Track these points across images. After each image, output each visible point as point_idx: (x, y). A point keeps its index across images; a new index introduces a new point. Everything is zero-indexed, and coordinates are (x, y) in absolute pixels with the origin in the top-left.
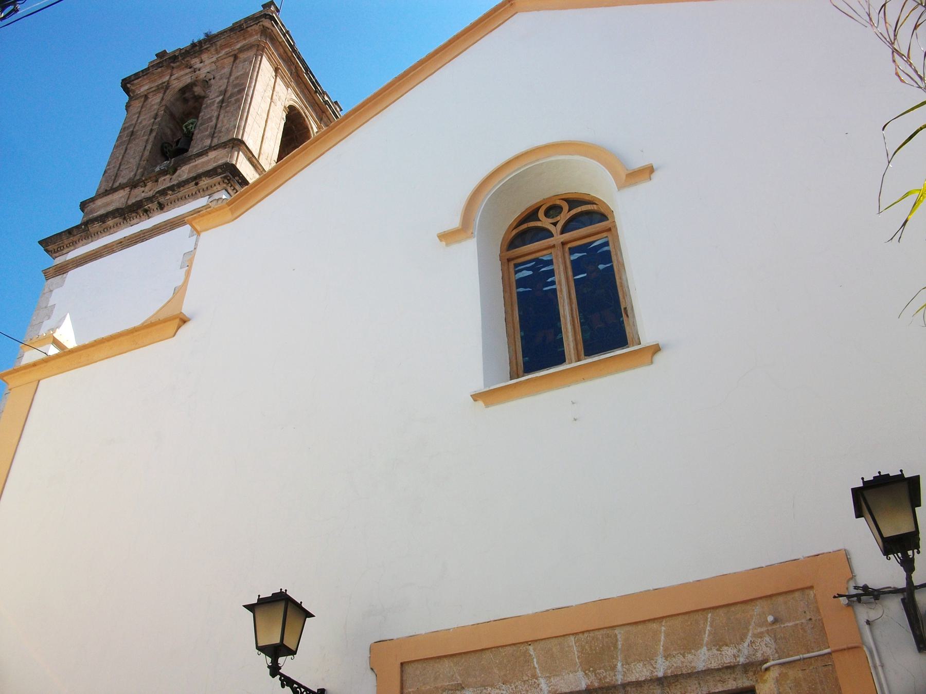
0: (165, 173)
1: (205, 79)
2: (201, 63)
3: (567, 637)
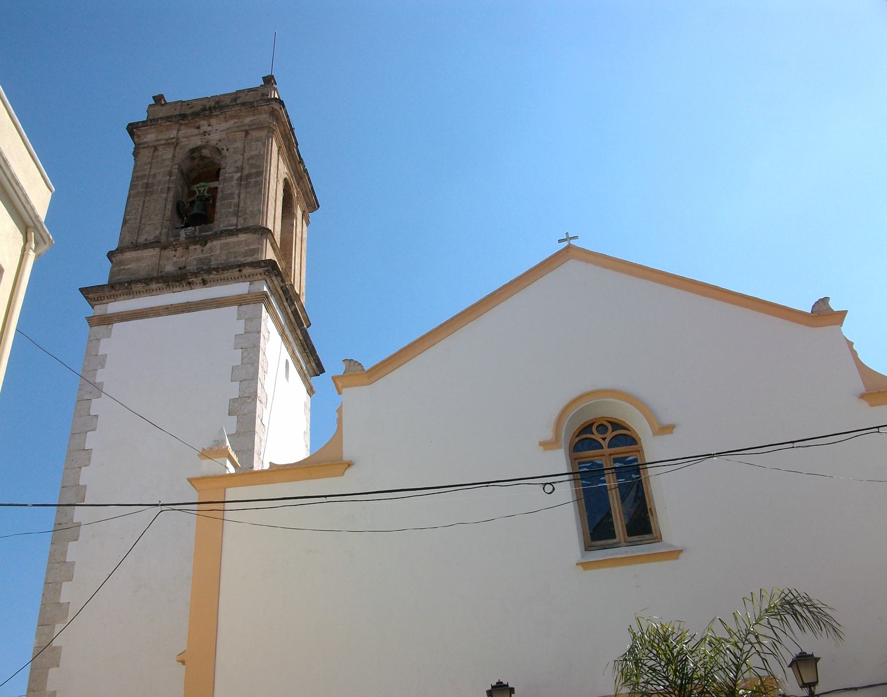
0: (196, 243)
2: (209, 126)
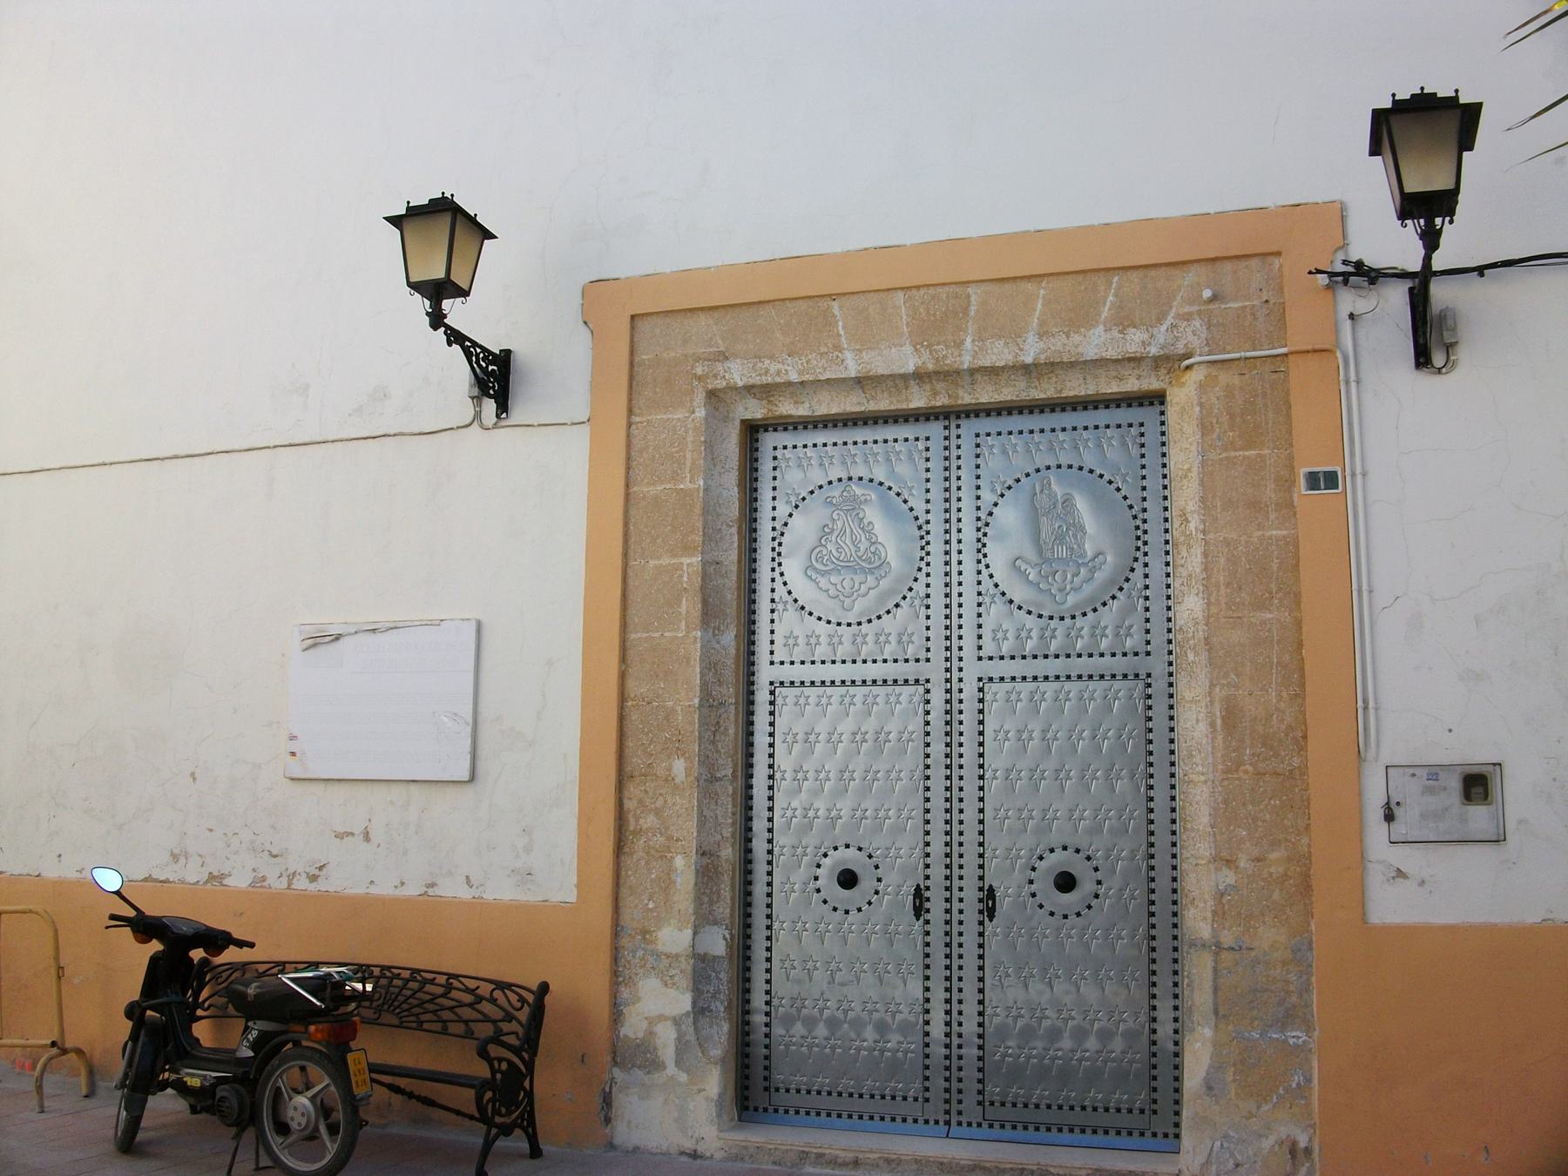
3: (894, 291)
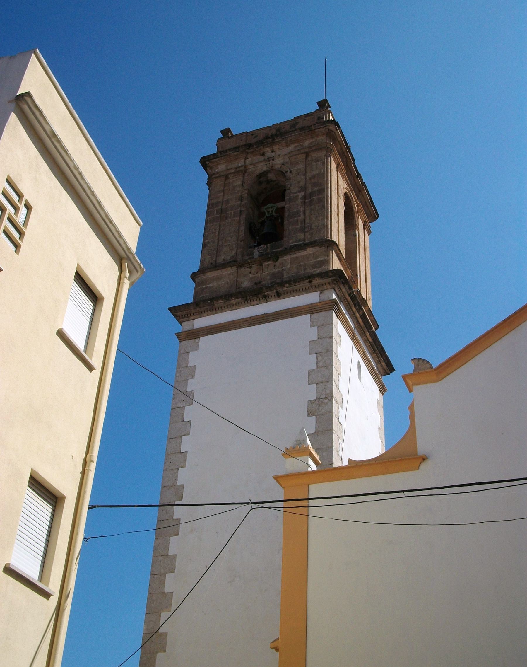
0: (268, 259)
1: (280, 170)
2: (272, 152)
